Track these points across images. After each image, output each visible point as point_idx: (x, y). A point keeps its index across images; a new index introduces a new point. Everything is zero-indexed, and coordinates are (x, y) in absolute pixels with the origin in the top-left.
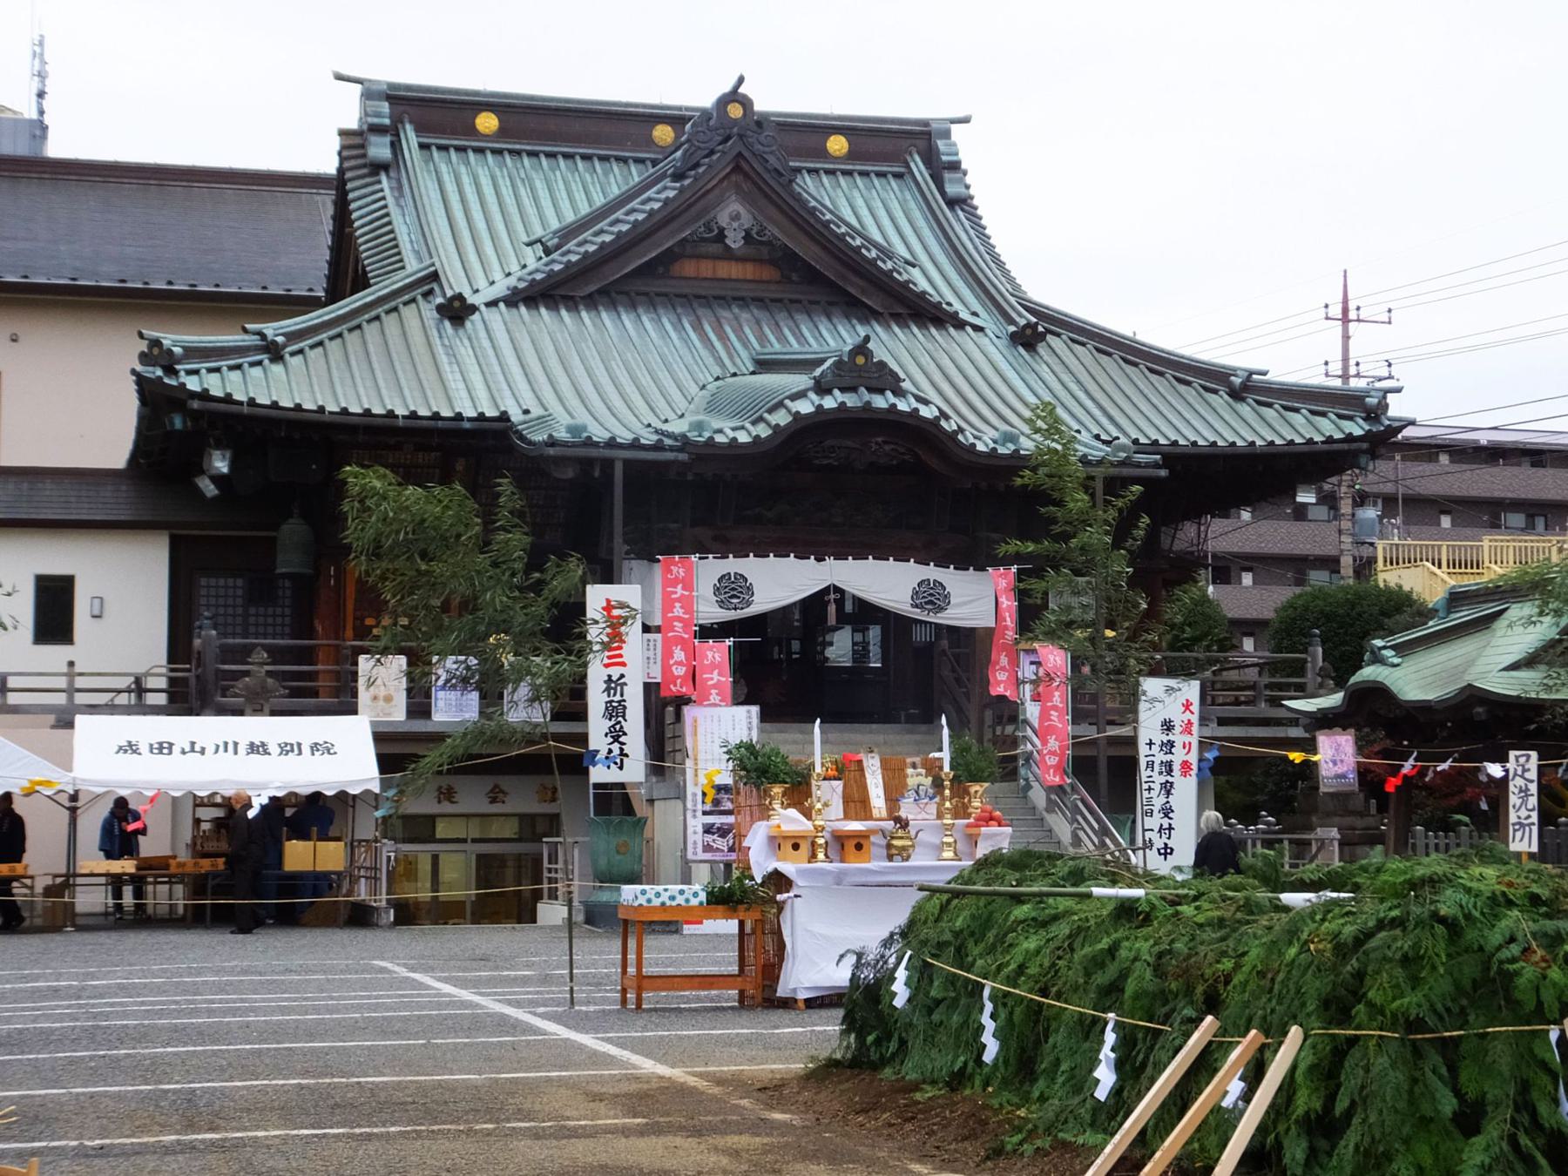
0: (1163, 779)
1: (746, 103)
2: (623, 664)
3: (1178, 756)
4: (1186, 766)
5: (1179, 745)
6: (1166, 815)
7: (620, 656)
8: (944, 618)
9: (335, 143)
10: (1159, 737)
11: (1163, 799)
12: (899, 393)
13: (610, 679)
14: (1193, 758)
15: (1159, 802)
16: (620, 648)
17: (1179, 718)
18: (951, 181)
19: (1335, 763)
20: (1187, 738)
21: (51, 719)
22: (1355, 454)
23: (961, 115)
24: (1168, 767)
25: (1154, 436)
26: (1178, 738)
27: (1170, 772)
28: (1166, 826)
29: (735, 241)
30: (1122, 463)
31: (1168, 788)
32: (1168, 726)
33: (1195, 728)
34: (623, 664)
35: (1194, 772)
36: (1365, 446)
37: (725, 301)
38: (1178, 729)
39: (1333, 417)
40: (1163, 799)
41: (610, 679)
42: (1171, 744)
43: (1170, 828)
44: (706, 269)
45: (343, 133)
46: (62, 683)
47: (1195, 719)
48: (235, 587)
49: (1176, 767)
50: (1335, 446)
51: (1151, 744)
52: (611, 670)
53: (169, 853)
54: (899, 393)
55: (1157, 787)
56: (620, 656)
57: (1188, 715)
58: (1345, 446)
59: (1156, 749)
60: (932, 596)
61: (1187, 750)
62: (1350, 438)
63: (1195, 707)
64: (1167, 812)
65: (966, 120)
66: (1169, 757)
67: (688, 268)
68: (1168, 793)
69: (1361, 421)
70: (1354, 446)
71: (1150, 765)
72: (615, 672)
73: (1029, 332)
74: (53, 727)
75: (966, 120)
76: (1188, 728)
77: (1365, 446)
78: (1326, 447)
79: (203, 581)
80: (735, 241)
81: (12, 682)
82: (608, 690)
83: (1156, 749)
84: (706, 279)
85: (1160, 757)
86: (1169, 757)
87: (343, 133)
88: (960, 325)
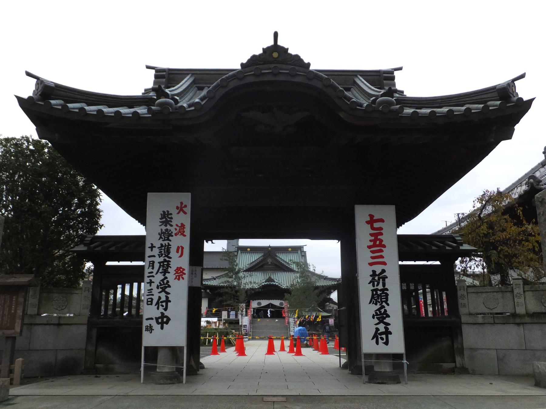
2: (384, 263)
7: (382, 257)
8: (262, 305)
9: (286, 47)
12: (274, 282)
13: (374, 273)
16: (381, 251)
29: (270, 263)
34: (384, 263)
37: (269, 270)
41: (374, 273)
44: (267, 266)
45: (288, 49)
49: (173, 250)
52: (375, 267)
53: (205, 267)
54: (274, 282)
56: (382, 257)
60: (281, 304)
65: (400, 69)
67: (265, 266)
72: (378, 269)
75: (400, 69)
80: (270, 263)
82: (372, 282)
87: (288, 49)
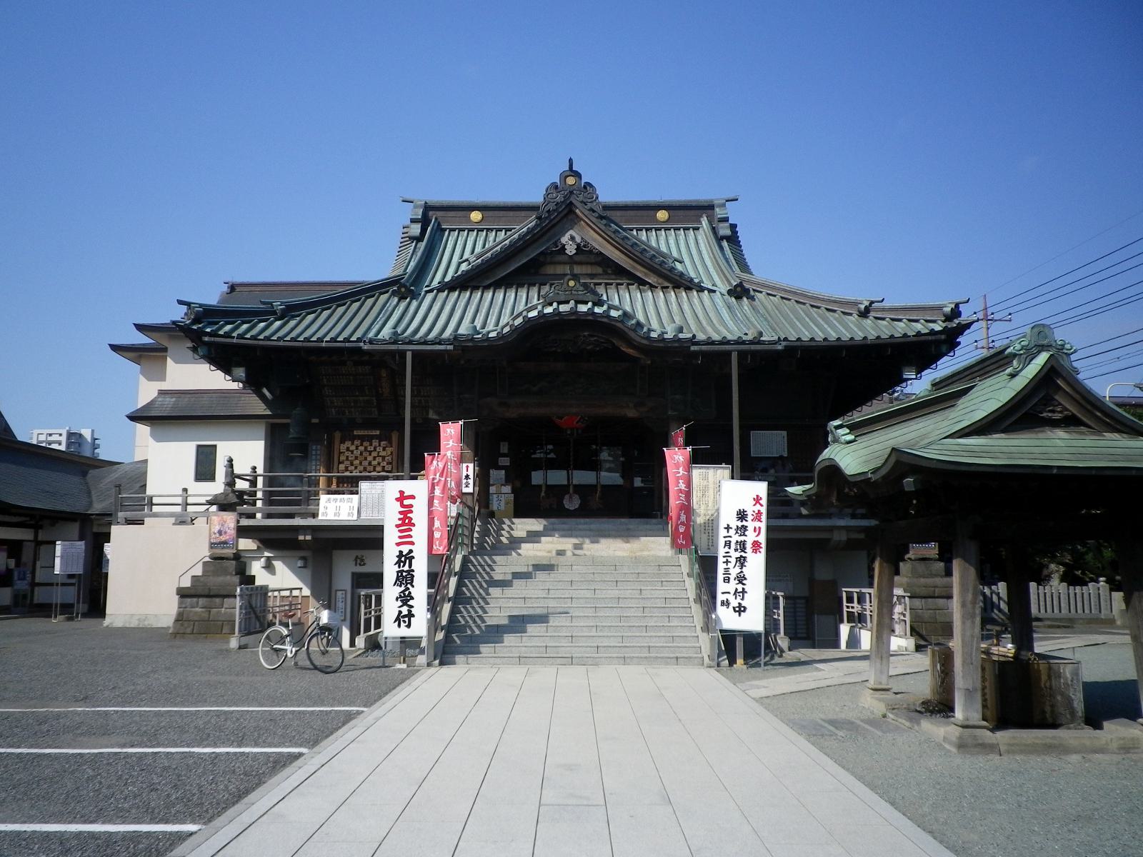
0: (738, 554)
1: (577, 175)
3: (750, 537)
4: (756, 545)
5: (750, 529)
6: (740, 582)
10: (735, 523)
11: (737, 570)
14: (762, 539)
15: (734, 572)
17: (750, 509)
18: (722, 228)
19: (220, 534)
20: (757, 524)
21: (173, 520)
22: (938, 343)
23: (731, 196)
24: (742, 546)
25: (692, 275)
26: (750, 524)
27: (743, 550)
28: (740, 590)
30: (751, 342)
31: (742, 561)
32: (742, 515)
33: (764, 517)
35: (763, 550)
36: (943, 337)
38: (750, 518)
39: (922, 321)
40: (737, 570)
42: (745, 528)
43: (744, 591)
46: (179, 500)
47: (764, 510)
48: (316, 450)
49: (749, 546)
50: (923, 338)
51: (728, 528)
55: (733, 560)
57: (758, 507)
58: (930, 338)
59: (732, 532)
61: (757, 532)
62: (932, 332)
63: (764, 502)
64: (741, 579)
66: (743, 538)
68: (742, 565)
69: (941, 323)
70: (938, 337)
71: (728, 544)
73: (739, 289)
74: (174, 524)
76: (758, 517)
77: (943, 337)
78: (915, 339)
79: (314, 447)
81: (155, 500)
83: (732, 532)
84: (550, 275)
85: (736, 539)
86: (743, 538)
88: (701, 289)
